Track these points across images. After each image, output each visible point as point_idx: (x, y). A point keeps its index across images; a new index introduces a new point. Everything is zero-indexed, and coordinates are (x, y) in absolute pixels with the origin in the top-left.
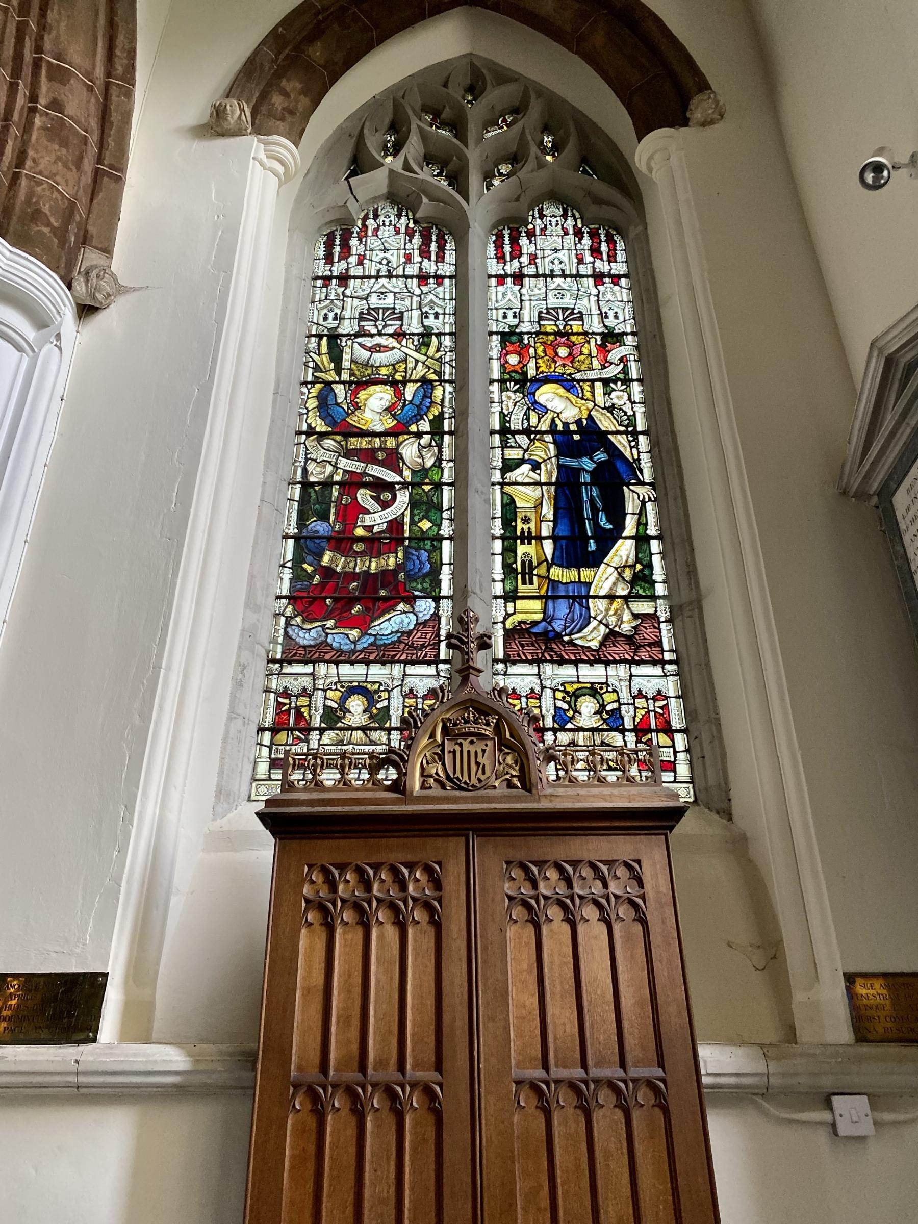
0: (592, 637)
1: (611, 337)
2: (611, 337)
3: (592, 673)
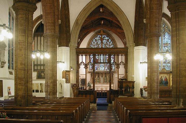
0: (167, 62)
1: (169, 44)
2: (169, 44)
3: (167, 64)
